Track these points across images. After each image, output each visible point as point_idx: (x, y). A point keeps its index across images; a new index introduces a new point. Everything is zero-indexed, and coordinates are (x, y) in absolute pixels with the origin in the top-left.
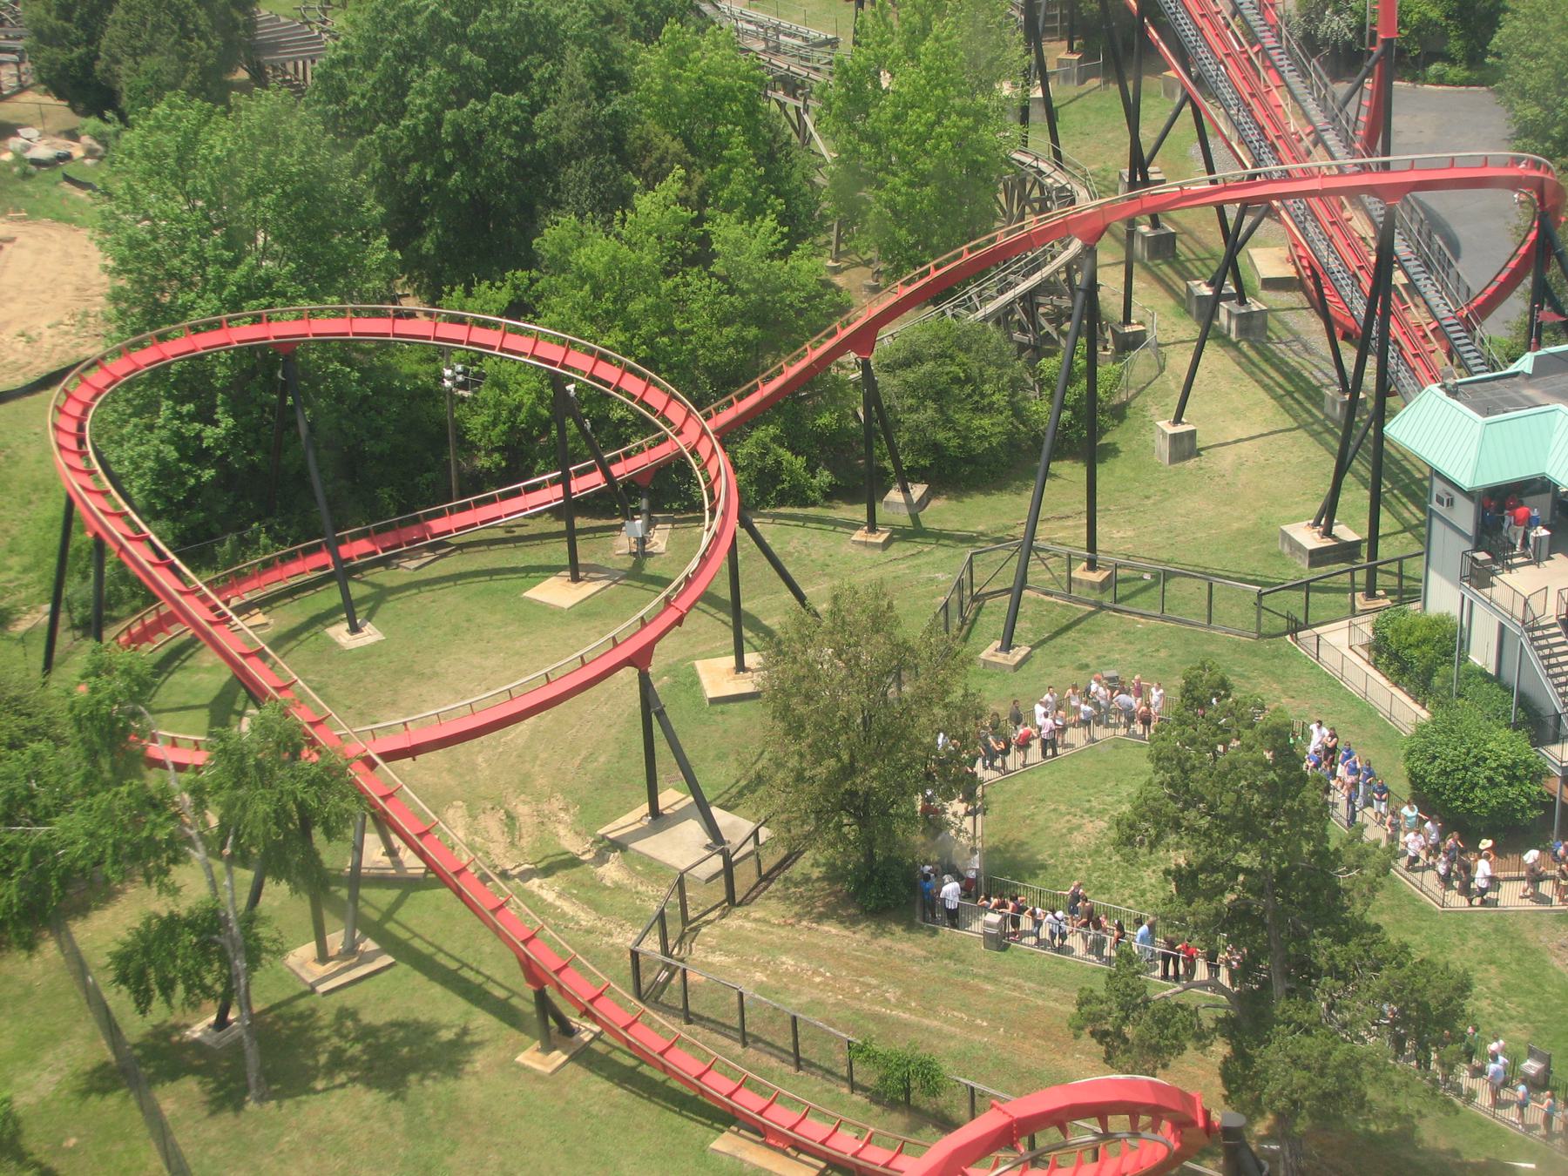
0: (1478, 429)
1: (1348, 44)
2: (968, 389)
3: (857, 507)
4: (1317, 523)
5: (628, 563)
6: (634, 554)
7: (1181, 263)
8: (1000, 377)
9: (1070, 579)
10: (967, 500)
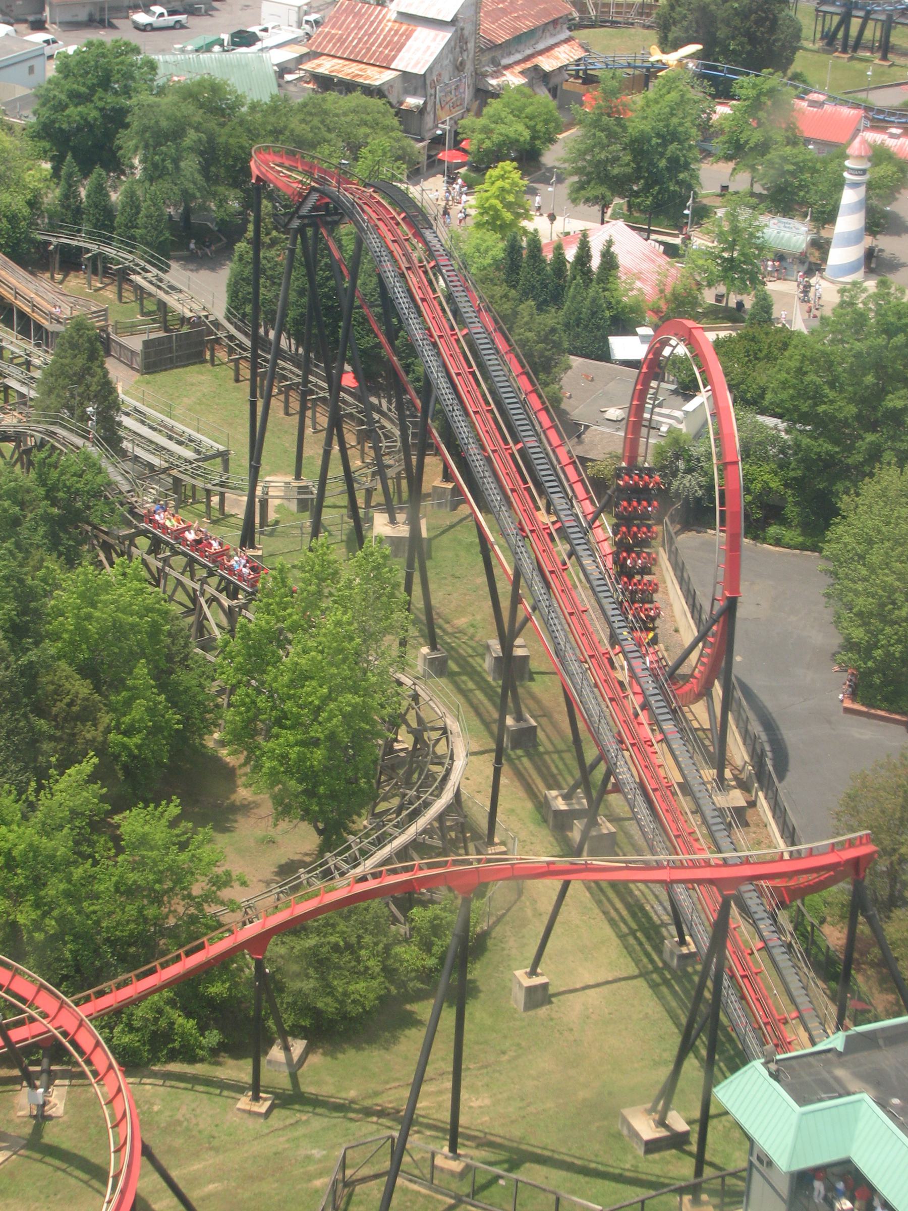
0: (794, 1119)
1: (698, 500)
2: (347, 957)
3: (242, 1062)
4: (653, 1109)
5: (27, 1130)
6: (35, 1117)
7: (540, 755)
8: (376, 944)
9: (433, 1166)
10: (340, 1056)
